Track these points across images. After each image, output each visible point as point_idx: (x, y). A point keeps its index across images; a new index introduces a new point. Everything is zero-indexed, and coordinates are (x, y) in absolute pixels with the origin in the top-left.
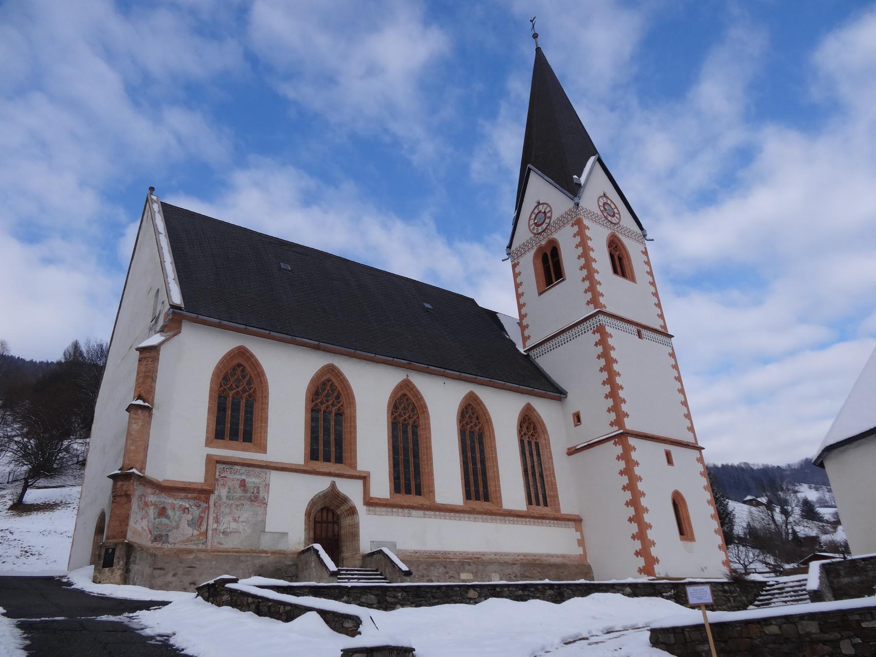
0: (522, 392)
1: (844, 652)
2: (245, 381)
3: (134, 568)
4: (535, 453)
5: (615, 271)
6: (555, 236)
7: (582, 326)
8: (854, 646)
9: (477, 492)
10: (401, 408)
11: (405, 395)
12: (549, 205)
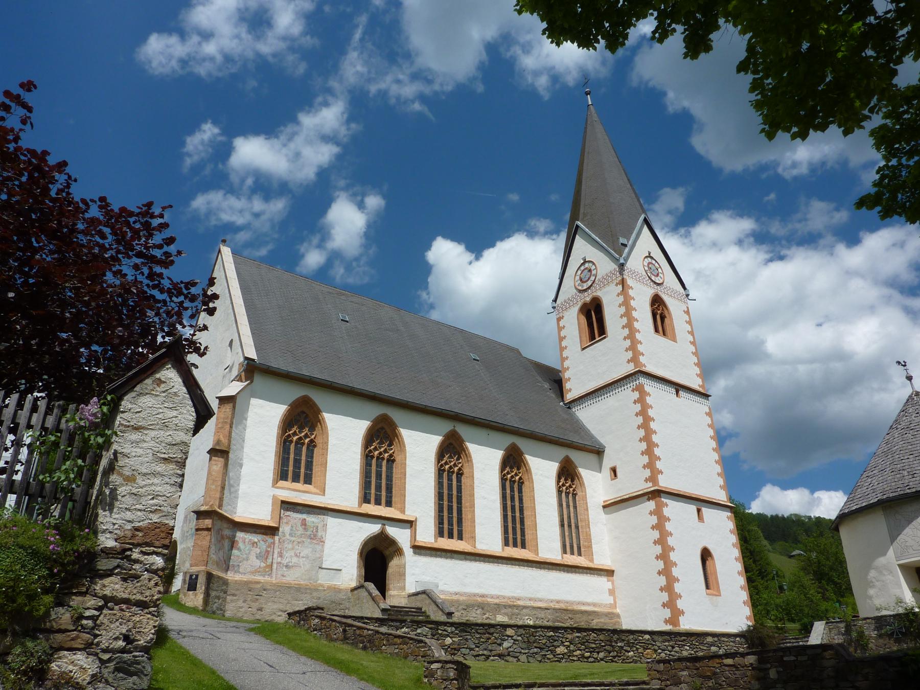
5: (657, 330)
9: (515, 540)
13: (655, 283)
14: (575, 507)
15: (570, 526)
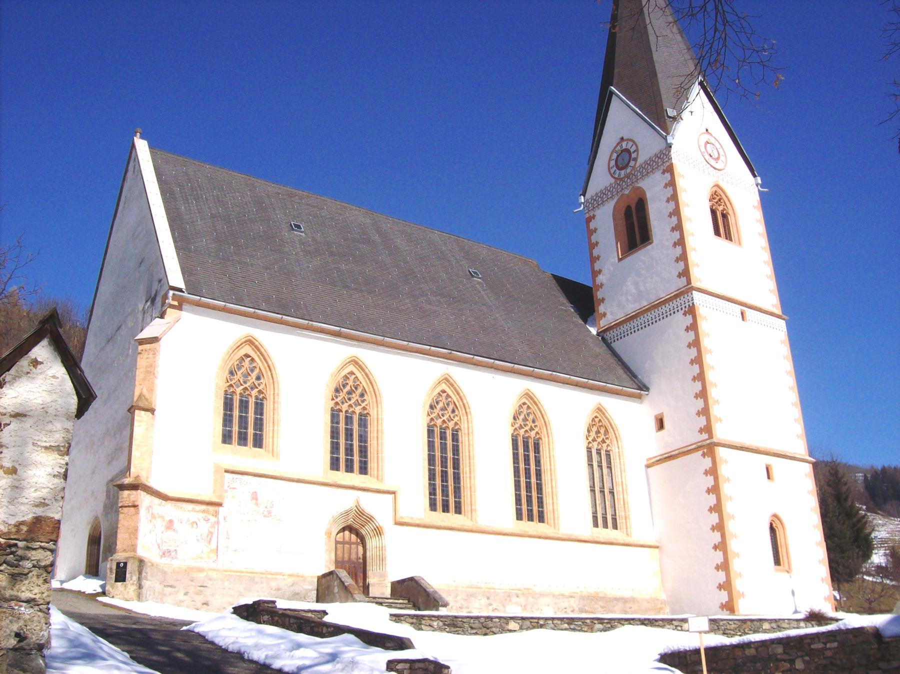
0: (592, 388)
1: (797, 667)
2: (254, 375)
3: (146, 584)
4: (604, 464)
5: (717, 233)
6: (642, 184)
7: (671, 305)
8: (804, 661)
9: (530, 512)
10: (438, 407)
11: (444, 391)
12: (634, 142)
13: (715, 169)
14: (610, 468)
15: (602, 492)
